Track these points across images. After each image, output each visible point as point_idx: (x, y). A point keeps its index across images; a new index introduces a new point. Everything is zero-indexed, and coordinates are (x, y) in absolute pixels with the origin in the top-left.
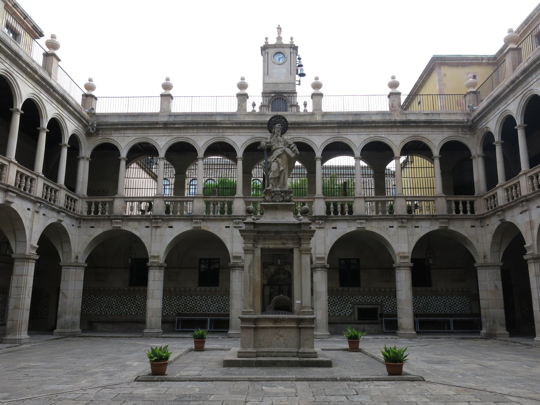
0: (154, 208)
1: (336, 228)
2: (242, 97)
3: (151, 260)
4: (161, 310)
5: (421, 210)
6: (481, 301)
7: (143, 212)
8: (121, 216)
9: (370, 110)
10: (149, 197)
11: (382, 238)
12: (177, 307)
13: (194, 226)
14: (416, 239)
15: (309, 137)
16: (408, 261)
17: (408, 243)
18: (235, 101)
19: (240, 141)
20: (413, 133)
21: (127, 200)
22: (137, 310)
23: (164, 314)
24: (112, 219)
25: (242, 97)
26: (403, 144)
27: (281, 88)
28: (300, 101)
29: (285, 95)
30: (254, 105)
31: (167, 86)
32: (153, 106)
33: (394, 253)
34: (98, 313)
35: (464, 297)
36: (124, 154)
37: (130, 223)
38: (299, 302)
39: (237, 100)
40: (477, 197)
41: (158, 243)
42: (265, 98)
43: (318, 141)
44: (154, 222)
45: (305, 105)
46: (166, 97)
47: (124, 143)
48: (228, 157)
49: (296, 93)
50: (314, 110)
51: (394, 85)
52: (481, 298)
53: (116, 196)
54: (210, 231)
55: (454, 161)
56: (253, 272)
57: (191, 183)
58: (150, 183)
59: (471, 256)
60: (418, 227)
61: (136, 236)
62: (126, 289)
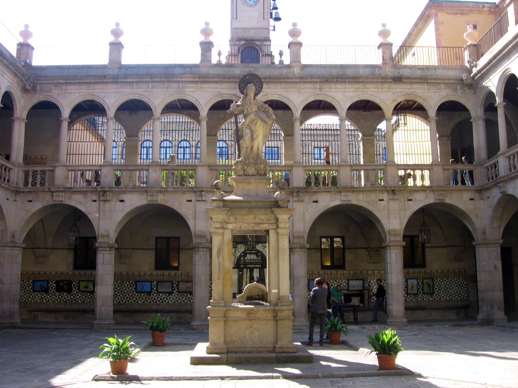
0: (103, 180)
1: (317, 202)
2: (207, 47)
3: (100, 240)
4: (112, 297)
5: (415, 180)
6: (478, 283)
7: (89, 182)
8: (64, 188)
9: (357, 64)
10: (95, 166)
11: (371, 213)
12: (130, 294)
13: (149, 198)
14: (409, 214)
15: (285, 94)
16: (400, 238)
17: (400, 218)
18: (198, 51)
19: (204, 98)
20: (407, 90)
21: (70, 168)
22: (84, 297)
23: (115, 302)
24: (52, 192)
25: (207, 47)
26: (395, 104)
27: (251, 34)
28: (275, 50)
29: (258, 43)
30: (219, 54)
31: (117, 33)
32: (100, 57)
33: (384, 230)
34: (39, 301)
35: (461, 279)
36: (66, 113)
37: (74, 196)
38: (276, 291)
39: (200, 49)
40: (477, 165)
41: (107, 220)
42: (233, 47)
43: (297, 98)
44: (151, 195)
45: (281, 54)
46: (116, 47)
47: (67, 102)
48: (189, 116)
49: (270, 41)
50: (291, 62)
51: (384, 33)
52: (478, 280)
53: (57, 164)
54: (168, 205)
55: (453, 123)
56: (223, 258)
57: (180, 146)
58: (97, 147)
59: (469, 232)
60: (411, 200)
61: (80, 211)
62: (70, 273)
